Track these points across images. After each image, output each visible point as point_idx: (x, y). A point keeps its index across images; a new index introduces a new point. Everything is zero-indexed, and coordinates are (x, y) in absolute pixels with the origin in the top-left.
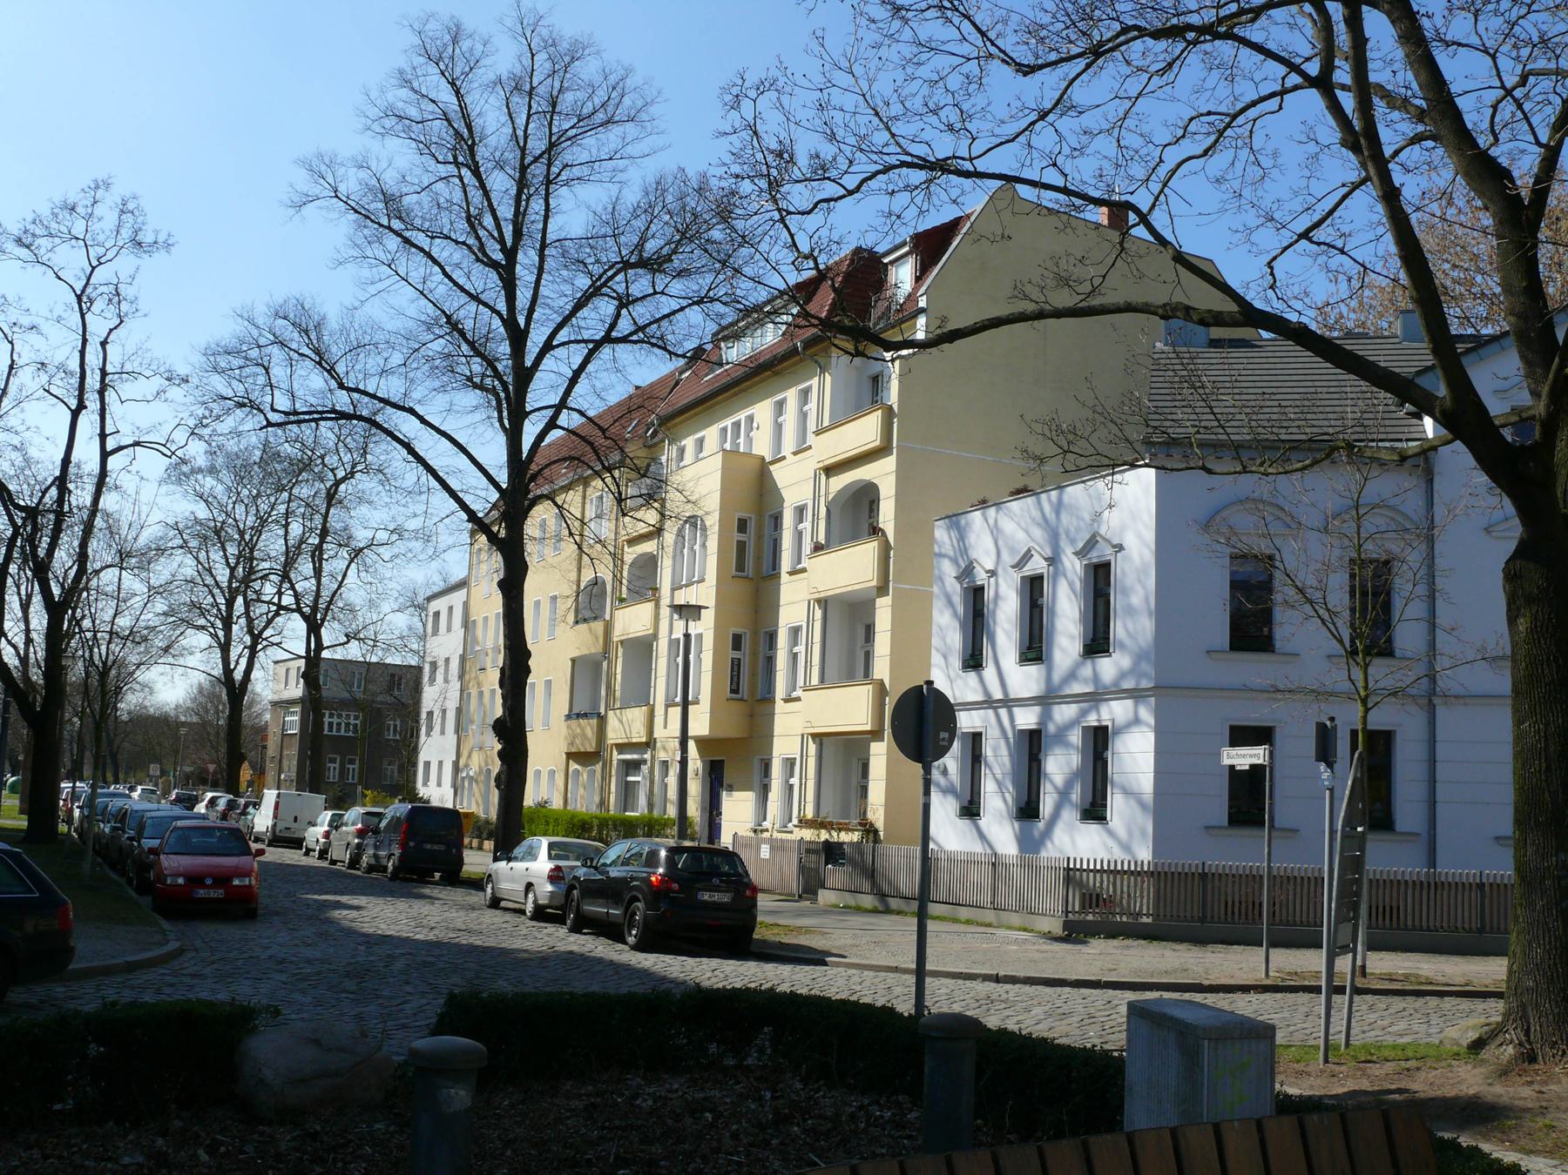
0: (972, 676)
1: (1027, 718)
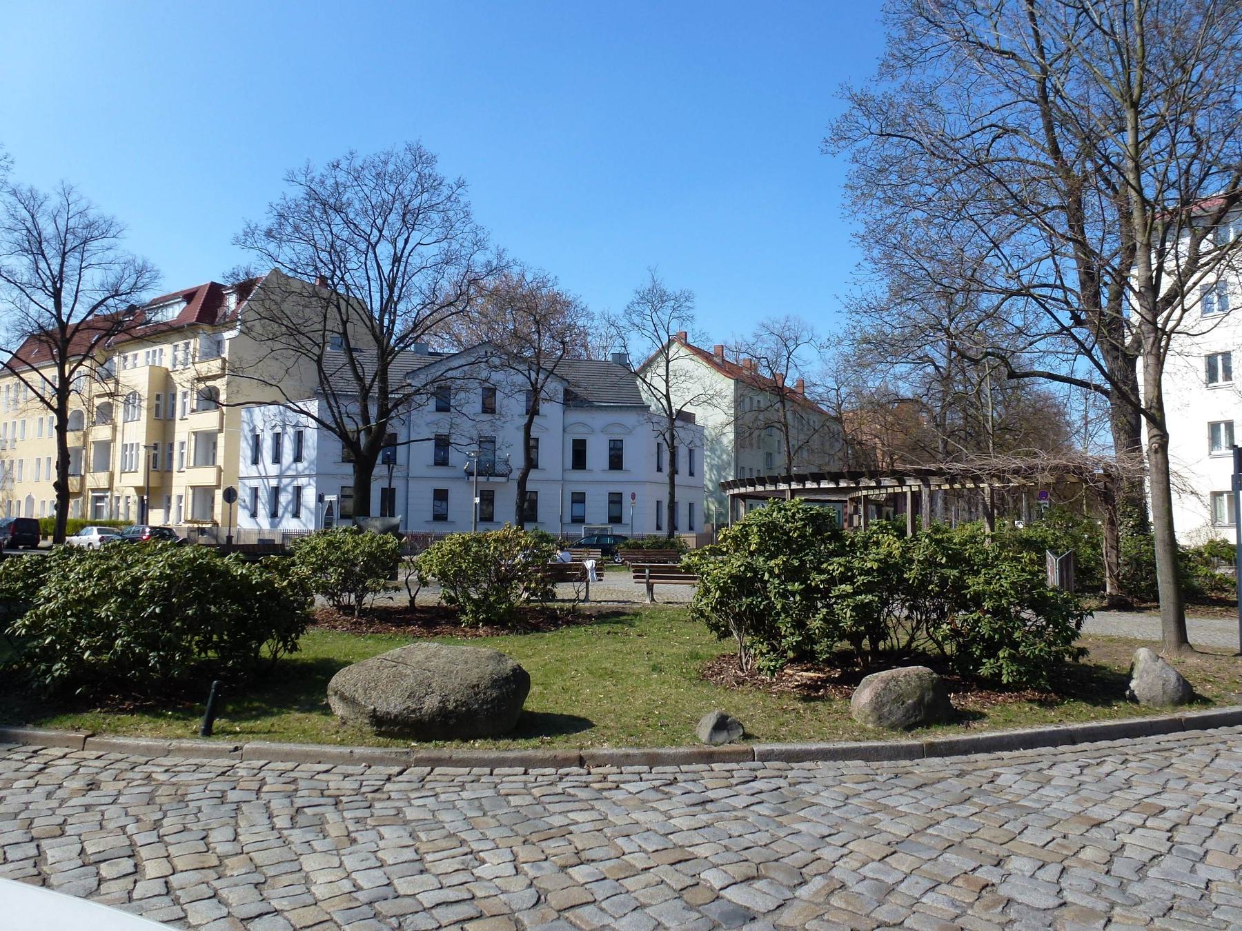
1: (274, 483)
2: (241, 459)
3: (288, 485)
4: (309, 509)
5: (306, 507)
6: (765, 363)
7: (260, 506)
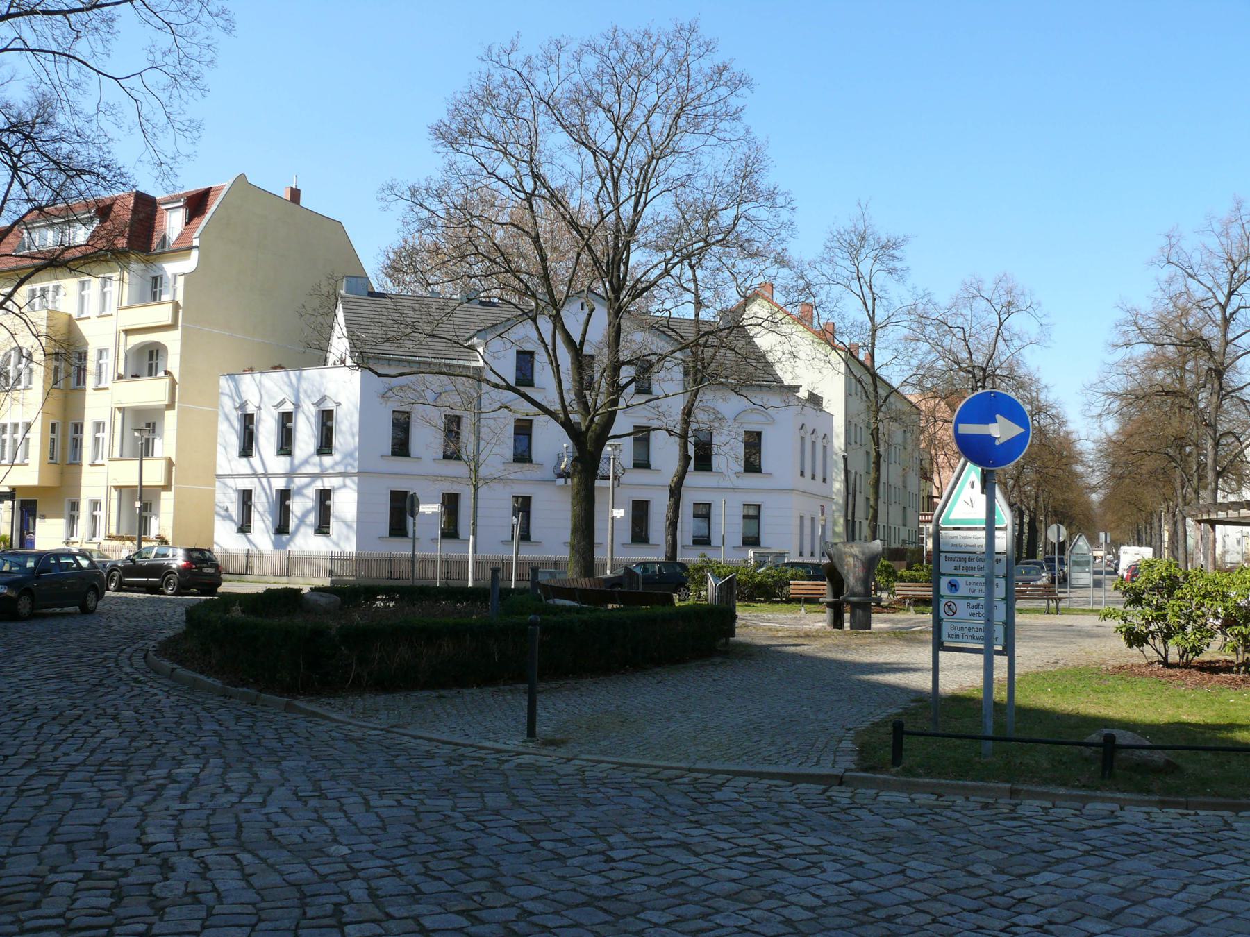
0: (244, 460)
1: (280, 484)
2: (220, 449)
4: (345, 522)
6: (960, 335)
7: (255, 516)
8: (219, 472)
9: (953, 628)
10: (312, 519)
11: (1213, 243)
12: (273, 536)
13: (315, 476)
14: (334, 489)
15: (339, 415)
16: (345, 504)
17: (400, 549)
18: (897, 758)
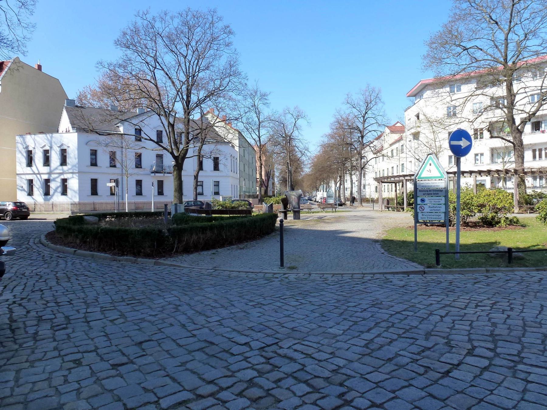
0: (29, 168)
1: (46, 177)
2: (17, 164)
3: (57, 177)
4: (74, 191)
5: (71, 190)
7: (35, 189)
8: (18, 173)
9: (423, 215)
10: (60, 190)
11: (362, 97)
12: (43, 197)
13: (61, 174)
14: (69, 179)
15: (69, 151)
16: (73, 184)
17: (94, 199)
18: (438, 262)
